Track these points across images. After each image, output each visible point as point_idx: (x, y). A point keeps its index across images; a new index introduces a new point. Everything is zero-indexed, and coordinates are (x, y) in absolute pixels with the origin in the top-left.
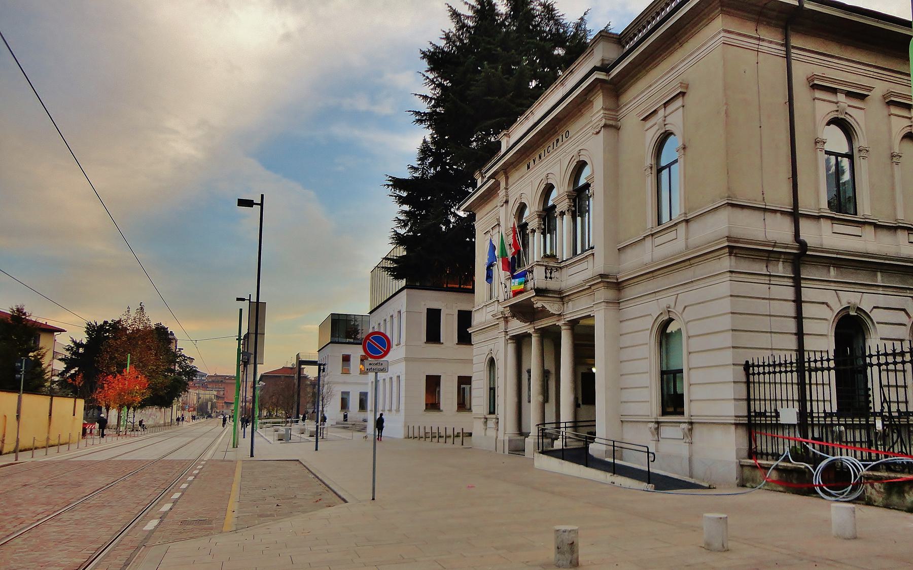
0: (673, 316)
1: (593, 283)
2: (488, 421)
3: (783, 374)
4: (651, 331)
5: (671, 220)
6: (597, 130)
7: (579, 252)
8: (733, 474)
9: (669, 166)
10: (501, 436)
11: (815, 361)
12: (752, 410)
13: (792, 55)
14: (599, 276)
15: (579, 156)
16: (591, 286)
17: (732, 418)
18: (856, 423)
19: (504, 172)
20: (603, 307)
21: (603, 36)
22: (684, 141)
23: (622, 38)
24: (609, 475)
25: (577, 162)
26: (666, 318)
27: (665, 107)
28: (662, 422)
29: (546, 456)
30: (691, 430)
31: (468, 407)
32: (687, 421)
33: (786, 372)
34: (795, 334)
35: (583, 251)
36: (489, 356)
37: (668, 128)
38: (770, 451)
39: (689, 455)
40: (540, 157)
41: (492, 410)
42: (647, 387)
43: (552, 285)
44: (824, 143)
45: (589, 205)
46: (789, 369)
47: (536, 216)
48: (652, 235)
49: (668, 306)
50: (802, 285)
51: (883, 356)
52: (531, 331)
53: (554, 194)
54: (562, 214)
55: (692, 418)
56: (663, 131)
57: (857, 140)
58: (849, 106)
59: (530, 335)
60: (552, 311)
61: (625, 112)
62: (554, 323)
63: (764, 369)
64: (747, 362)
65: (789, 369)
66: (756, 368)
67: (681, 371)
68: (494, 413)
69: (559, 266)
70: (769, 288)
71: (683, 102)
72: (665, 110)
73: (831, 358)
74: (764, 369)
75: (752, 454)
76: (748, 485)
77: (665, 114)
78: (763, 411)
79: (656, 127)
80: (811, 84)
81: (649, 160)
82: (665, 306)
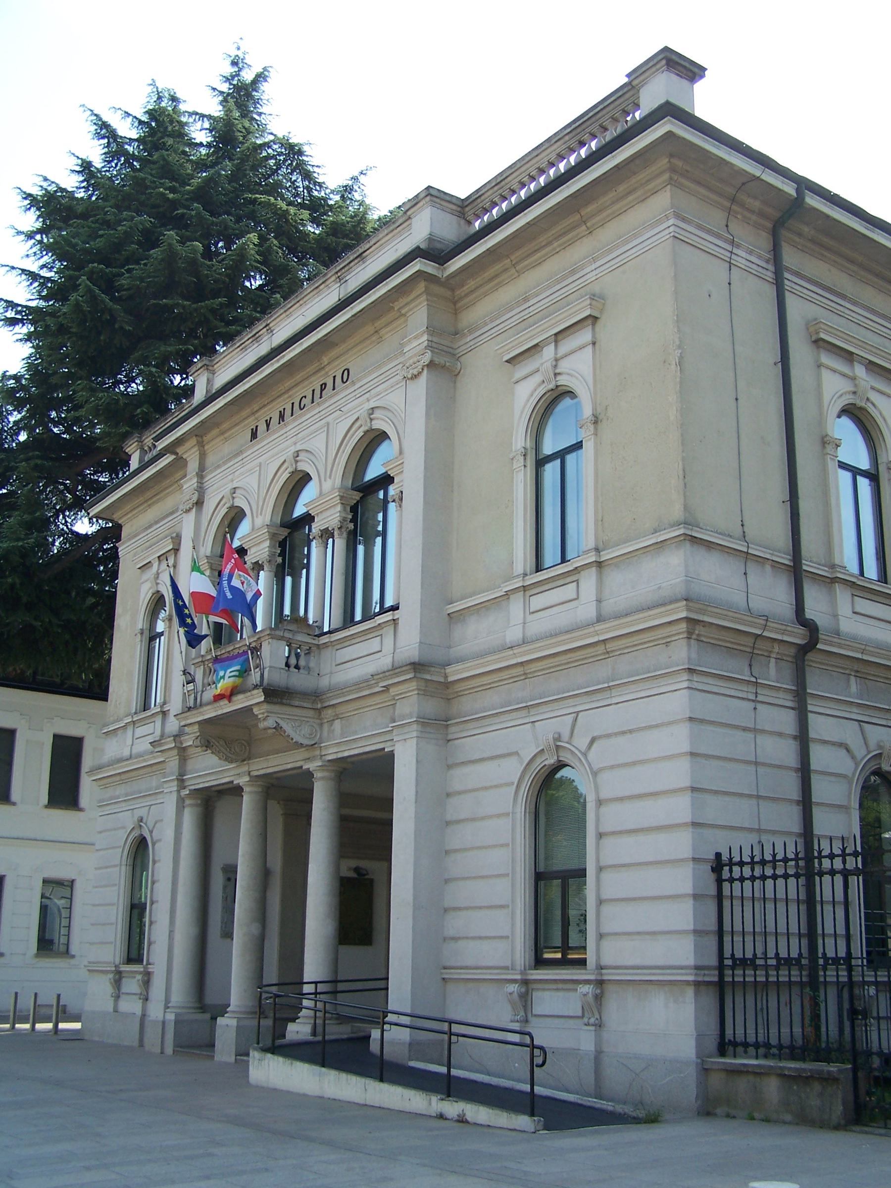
0: (565, 757)
1: (396, 680)
2: (124, 980)
3: (780, 882)
4: (518, 787)
5: (564, 560)
6: (415, 372)
7: (358, 617)
8: (689, 1093)
9: (561, 455)
10: (156, 1011)
11: (832, 856)
12: (727, 953)
13: (786, 282)
14: (408, 667)
15: (371, 420)
16: (387, 688)
17: (688, 971)
18: (881, 980)
19: (428, 305)
20: (415, 734)
21: (432, 195)
22: (594, 409)
23: (466, 206)
24: (434, 1099)
25: (366, 432)
26: (551, 761)
27: (556, 342)
28: (536, 981)
29: (281, 1059)
30: (599, 998)
31: (62, 948)
32: (592, 977)
33: (775, 877)
34: (798, 802)
35: (367, 617)
36: (135, 833)
37: (562, 380)
38: (751, 1039)
39: (596, 1051)
40: (282, 417)
41: (134, 955)
42: (502, 907)
43: (298, 680)
44: (838, 446)
45: (308, 556)
46: (780, 871)
47: (267, 536)
48: (525, 588)
49: (556, 736)
50: (810, 708)
51: (852, 857)
52: (242, 781)
53: (244, 528)
54: (327, 534)
55: (604, 971)
56: (552, 386)
57: (884, 450)
58: (873, 388)
59: (237, 791)
60: (298, 738)
61: (468, 345)
62: (298, 764)
63: (753, 870)
64: (718, 855)
65: (780, 871)
66: (736, 869)
67: (582, 873)
68: (139, 960)
69: (316, 642)
70: (755, 709)
71: (594, 336)
72: (593, 329)
73: (836, 853)
74: (753, 870)
75: (724, 1046)
76: (719, 1111)
77: (556, 354)
78: (749, 955)
79: (537, 378)
80: (813, 338)
81: (520, 440)
82: (551, 737)
